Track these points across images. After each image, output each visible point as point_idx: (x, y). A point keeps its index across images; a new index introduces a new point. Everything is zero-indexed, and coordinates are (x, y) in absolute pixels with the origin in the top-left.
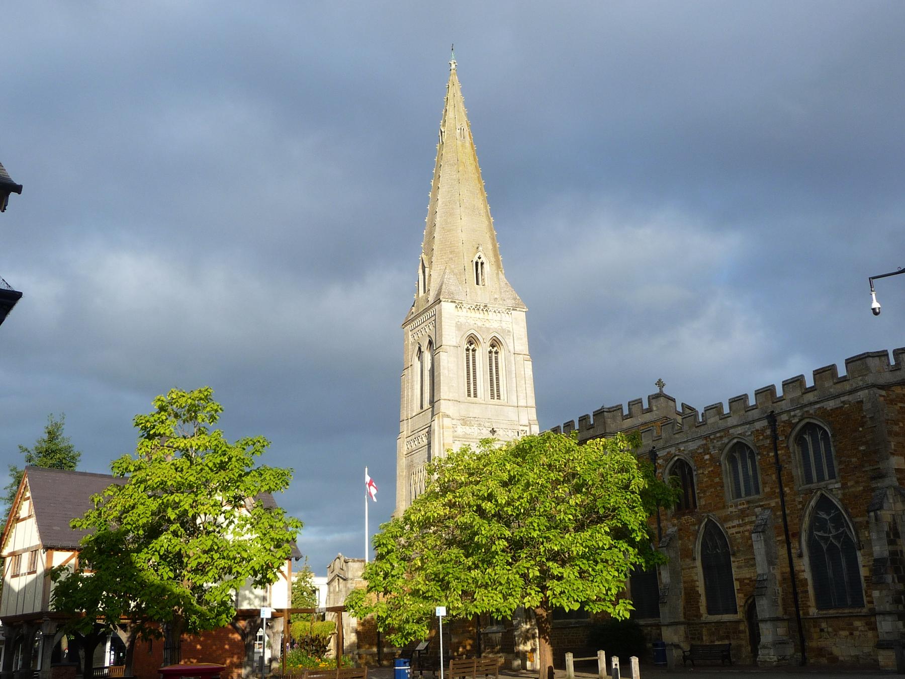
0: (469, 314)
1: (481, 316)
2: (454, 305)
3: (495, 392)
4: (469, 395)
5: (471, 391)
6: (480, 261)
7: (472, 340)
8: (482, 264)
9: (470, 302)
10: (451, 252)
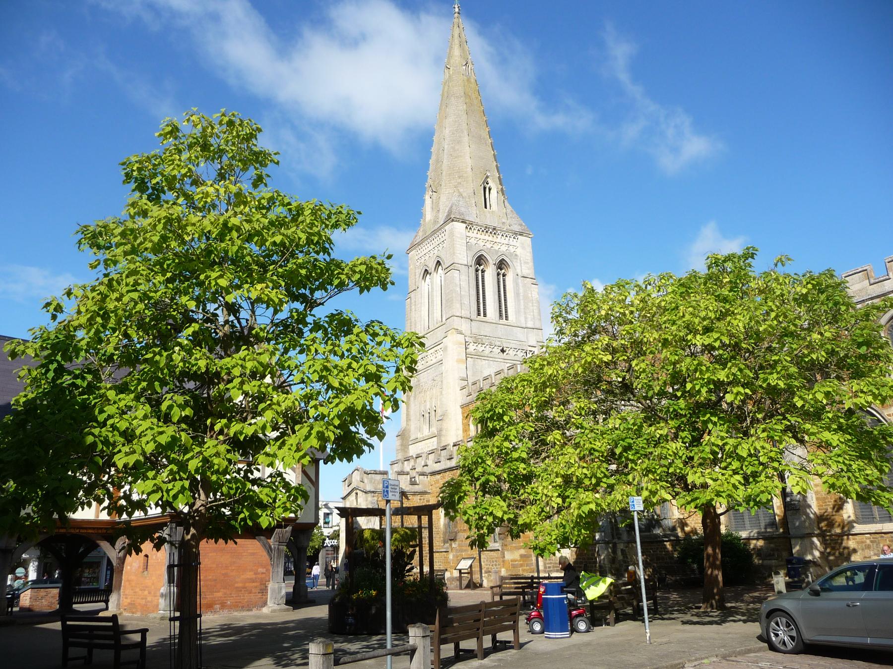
0: (479, 236)
1: (490, 238)
2: (464, 225)
3: (503, 313)
4: (479, 314)
5: (481, 310)
6: (488, 186)
7: (480, 260)
8: (490, 189)
9: (480, 223)
10: (459, 177)
